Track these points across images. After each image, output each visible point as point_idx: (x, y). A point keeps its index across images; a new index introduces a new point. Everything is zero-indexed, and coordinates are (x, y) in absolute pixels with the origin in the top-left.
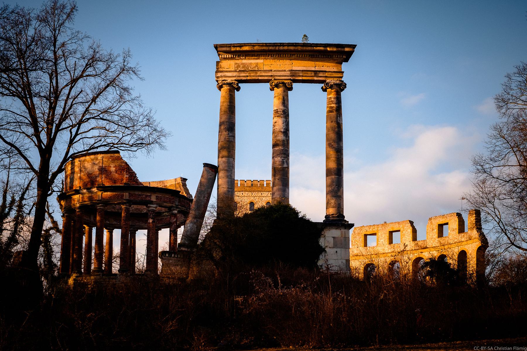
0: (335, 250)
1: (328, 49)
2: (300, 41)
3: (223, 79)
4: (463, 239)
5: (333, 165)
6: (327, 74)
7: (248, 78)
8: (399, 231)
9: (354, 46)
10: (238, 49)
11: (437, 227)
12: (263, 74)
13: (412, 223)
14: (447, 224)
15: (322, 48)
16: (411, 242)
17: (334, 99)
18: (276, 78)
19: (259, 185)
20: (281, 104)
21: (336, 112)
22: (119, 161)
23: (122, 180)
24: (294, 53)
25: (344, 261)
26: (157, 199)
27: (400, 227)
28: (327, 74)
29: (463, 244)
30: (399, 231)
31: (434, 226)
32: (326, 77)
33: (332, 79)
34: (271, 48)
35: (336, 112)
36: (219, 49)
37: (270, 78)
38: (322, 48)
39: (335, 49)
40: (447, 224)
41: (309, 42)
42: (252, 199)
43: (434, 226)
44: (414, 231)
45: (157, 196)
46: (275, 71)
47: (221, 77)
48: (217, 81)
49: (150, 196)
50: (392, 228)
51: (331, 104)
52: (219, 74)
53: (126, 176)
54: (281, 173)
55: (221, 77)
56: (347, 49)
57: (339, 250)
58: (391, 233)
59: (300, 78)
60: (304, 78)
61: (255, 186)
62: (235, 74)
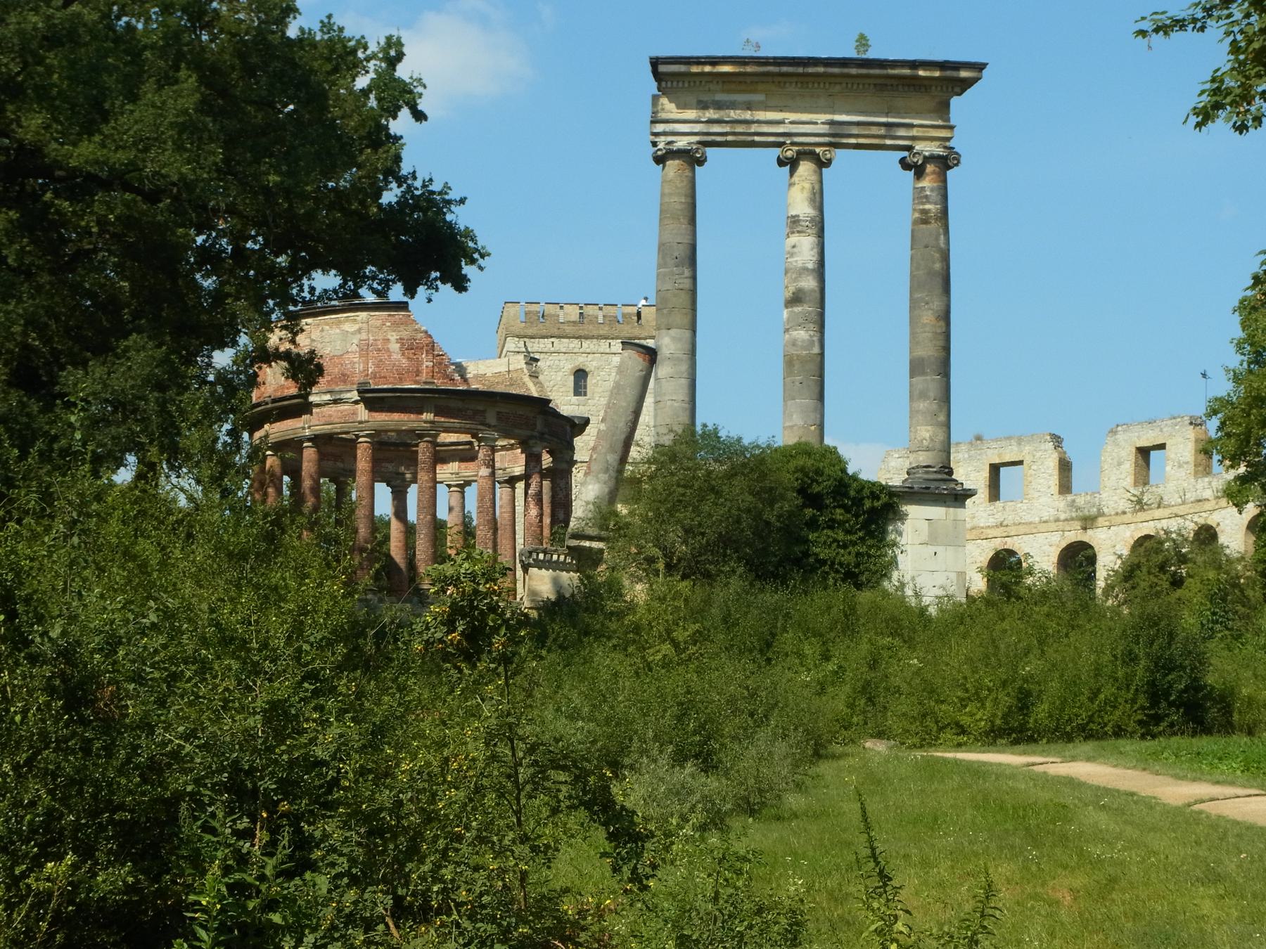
0: (934, 549)
1: (921, 73)
2: (851, 53)
3: (670, 139)
4: (1208, 494)
5: (929, 351)
6: (914, 132)
7: (730, 138)
8: (1020, 463)
9: (980, 67)
10: (707, 69)
11: (1132, 457)
12: (765, 129)
13: (1057, 440)
14: (1162, 447)
15: (907, 72)
16: (1056, 496)
17: (932, 190)
18: (797, 139)
19: (601, 321)
20: (806, 203)
21: (934, 222)
22: (410, 328)
23: (418, 373)
24: (838, 80)
25: (953, 576)
26: (499, 419)
27: (1024, 453)
28: (914, 132)
29: (1208, 506)
30: (1020, 463)
31: (1123, 454)
32: (914, 138)
33: (928, 143)
34: (785, 69)
35: (934, 222)
36: (662, 68)
37: (781, 139)
38: (907, 72)
39: (937, 74)
40: (1162, 447)
41: (871, 55)
42: (580, 361)
43: (1123, 454)
44: (1065, 467)
45: (498, 413)
46: (791, 123)
47: (665, 134)
48: (654, 144)
49: (484, 411)
50: (999, 455)
51: (923, 204)
52: (660, 128)
53: (427, 363)
54: (810, 374)
55: (665, 134)
56: (964, 74)
57: (940, 549)
58: (995, 469)
59: (853, 141)
60: (862, 141)
61: (591, 322)
62: (697, 128)
